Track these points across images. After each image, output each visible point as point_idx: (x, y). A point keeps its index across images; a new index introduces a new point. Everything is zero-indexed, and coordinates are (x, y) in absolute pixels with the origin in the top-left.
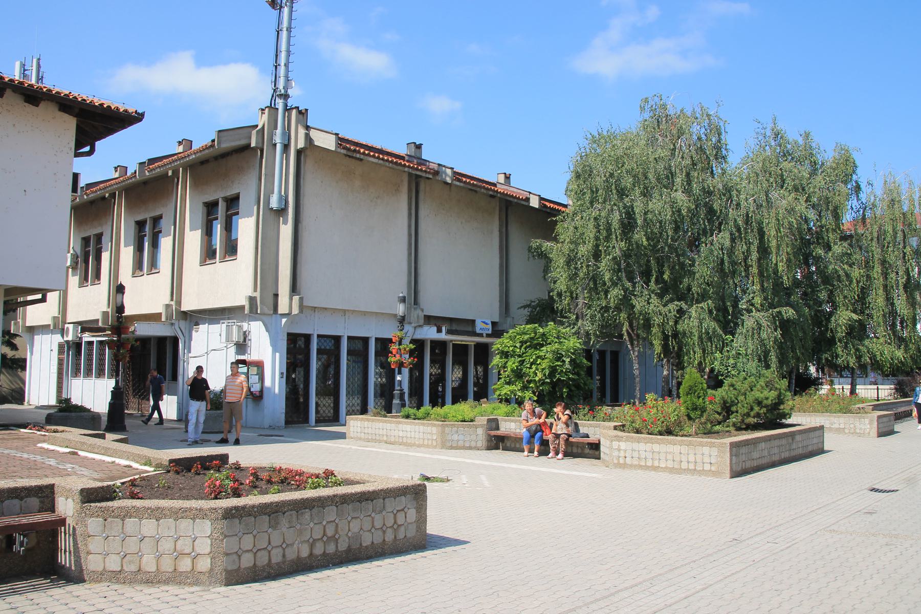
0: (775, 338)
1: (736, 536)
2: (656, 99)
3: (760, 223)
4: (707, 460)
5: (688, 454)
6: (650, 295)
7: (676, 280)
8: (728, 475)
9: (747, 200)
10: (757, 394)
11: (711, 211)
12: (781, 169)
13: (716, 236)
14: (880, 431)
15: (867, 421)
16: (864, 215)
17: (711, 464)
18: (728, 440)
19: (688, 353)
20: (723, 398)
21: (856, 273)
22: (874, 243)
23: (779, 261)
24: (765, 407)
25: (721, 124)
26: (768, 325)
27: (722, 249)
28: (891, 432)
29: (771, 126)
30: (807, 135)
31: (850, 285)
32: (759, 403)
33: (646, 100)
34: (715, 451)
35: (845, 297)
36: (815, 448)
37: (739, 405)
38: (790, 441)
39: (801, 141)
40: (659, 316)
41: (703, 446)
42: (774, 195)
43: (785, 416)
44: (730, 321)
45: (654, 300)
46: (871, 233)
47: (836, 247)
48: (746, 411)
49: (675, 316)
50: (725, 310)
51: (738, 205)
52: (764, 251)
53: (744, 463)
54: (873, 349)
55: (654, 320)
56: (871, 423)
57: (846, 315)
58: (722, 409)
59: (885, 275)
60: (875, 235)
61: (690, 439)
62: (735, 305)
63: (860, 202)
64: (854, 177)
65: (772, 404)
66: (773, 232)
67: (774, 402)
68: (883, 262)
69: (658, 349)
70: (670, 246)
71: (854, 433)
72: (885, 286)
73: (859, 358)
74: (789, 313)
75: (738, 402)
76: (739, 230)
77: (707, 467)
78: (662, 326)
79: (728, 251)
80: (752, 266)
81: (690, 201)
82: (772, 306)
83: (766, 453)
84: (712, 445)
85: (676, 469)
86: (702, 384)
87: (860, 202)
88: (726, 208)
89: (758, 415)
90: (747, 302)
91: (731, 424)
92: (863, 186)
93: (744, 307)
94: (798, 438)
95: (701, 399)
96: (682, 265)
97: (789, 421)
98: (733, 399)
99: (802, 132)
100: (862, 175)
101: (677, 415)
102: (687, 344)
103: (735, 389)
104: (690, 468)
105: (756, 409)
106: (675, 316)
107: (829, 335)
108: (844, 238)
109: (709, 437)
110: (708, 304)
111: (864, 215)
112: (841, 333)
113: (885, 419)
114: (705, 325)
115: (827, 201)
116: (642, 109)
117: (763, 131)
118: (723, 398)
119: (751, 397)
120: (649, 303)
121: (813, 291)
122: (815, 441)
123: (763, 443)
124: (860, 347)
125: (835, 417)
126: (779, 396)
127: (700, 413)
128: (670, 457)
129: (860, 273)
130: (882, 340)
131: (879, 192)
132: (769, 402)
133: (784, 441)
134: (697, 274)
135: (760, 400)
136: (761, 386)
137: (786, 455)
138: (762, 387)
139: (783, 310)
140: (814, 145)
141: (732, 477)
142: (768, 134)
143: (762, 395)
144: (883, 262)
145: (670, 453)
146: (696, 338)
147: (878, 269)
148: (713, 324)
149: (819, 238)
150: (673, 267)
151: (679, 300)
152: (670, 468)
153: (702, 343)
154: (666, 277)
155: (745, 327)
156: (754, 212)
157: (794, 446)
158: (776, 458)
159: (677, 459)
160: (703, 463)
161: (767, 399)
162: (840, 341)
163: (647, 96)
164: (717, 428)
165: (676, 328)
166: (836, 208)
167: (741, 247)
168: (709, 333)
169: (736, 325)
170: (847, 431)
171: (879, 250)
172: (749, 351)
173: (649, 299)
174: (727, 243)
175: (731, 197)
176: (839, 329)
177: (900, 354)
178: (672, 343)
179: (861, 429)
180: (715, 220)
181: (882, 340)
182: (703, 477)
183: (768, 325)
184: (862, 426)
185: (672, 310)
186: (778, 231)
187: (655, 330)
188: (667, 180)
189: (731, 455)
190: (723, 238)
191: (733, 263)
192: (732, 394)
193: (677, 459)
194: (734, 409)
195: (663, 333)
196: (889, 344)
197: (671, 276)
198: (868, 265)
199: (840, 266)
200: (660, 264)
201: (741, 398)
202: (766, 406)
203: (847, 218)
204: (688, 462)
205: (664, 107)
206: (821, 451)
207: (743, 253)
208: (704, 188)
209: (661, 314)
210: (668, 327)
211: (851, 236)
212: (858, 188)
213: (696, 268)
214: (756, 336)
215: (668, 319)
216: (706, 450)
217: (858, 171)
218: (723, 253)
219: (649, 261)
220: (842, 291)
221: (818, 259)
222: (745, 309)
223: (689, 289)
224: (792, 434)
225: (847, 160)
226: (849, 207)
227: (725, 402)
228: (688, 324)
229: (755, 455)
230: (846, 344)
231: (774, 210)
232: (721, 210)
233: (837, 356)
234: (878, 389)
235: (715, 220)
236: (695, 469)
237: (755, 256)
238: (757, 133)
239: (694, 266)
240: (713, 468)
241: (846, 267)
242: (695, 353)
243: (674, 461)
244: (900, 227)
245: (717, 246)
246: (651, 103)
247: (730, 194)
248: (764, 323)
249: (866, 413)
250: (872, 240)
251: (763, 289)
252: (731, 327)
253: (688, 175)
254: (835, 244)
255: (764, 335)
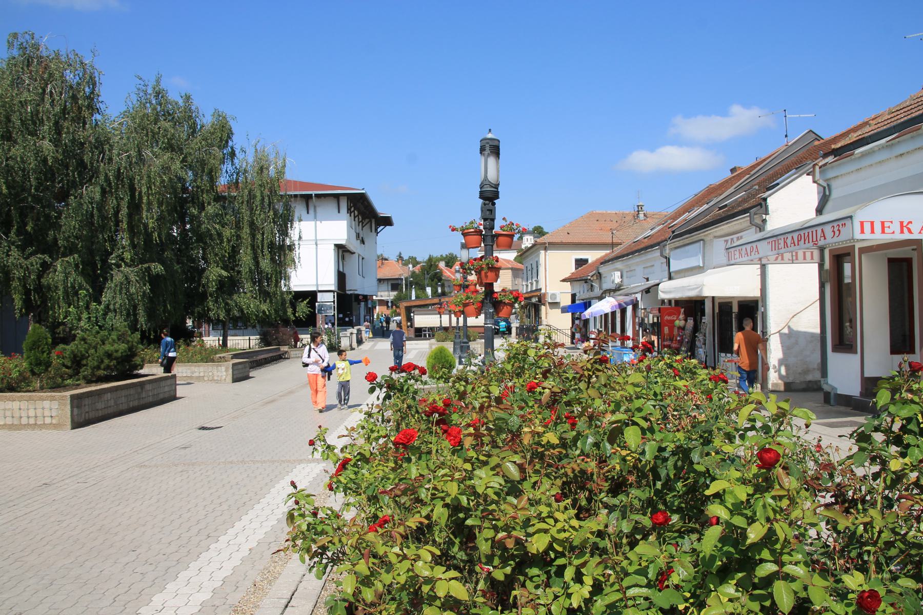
0: (144, 292)
1: (47, 481)
2: (27, 37)
3: (132, 180)
4: (47, 413)
5: (28, 409)
6: (9, 247)
7: (41, 231)
8: (69, 427)
9: (119, 155)
10: (108, 347)
11: (81, 164)
12: (159, 128)
13: (86, 189)
14: (235, 377)
15: (223, 369)
16: (237, 180)
17: (52, 417)
18: (68, 394)
19: (53, 308)
20: (73, 352)
21: (227, 232)
22: (244, 206)
23: (149, 218)
24: (115, 359)
25: (96, 74)
26: (136, 280)
27: (91, 203)
28: (247, 377)
29: (152, 83)
30: (188, 98)
31: (221, 243)
32: (109, 355)
33: (15, 36)
34: (55, 405)
35: (216, 255)
36: (166, 395)
37: (90, 358)
38: (139, 390)
39: (181, 102)
40: (20, 269)
41: (43, 400)
42: (147, 153)
43: (136, 367)
44: (99, 275)
45: (15, 252)
46: (242, 197)
47: (209, 207)
48: (96, 364)
49: (38, 269)
50: (94, 265)
51: (110, 159)
52: (135, 207)
53: (87, 415)
54: (240, 303)
55: (14, 274)
56: (226, 371)
57: (216, 271)
58: (73, 363)
59: (253, 236)
60: (246, 198)
61: (33, 394)
62: (104, 261)
63: (234, 167)
64: (230, 143)
65: (122, 356)
66: (144, 189)
67: (124, 354)
68: (252, 224)
69: (18, 302)
70: (33, 196)
71: (213, 380)
72: (253, 246)
73: (228, 311)
74: (157, 268)
75: (89, 356)
76: (110, 184)
77: (48, 420)
78: (23, 280)
79: (97, 205)
80: (122, 222)
81: (57, 151)
82: (142, 261)
83: (112, 403)
84: (52, 399)
85: (16, 425)
86: (46, 339)
87: (234, 167)
88: (98, 161)
89: (108, 367)
90: (117, 257)
91: (81, 377)
92: (237, 152)
93: (113, 262)
94: (148, 387)
95: (45, 354)
96: (48, 217)
97: (141, 372)
98: (84, 352)
99: (183, 94)
100: (237, 142)
101: (19, 371)
102: (52, 298)
103: (86, 343)
104: (31, 423)
105: (106, 361)
106: (38, 269)
107: (201, 289)
108: (219, 198)
109: (54, 392)
110: (74, 258)
111: (237, 180)
112: (212, 287)
113: (240, 366)
114: (71, 279)
115: (203, 163)
116: (10, 45)
117: (144, 88)
118: (73, 352)
119: (102, 350)
120: (8, 255)
121: (187, 248)
122: (167, 389)
123: (109, 394)
124: (229, 302)
125: (195, 366)
126: (130, 349)
127: (44, 368)
128: (8, 413)
129: (231, 233)
130: (249, 295)
131: (251, 159)
132: (119, 354)
133: (132, 391)
134: (63, 228)
135: (110, 352)
136: (112, 339)
137: (136, 403)
138: (114, 340)
139: (153, 265)
140: (193, 108)
141: (73, 428)
142: (150, 91)
143: (112, 348)
144: (252, 224)
145: (9, 409)
146: (60, 293)
147: (246, 230)
148: (80, 279)
149: (195, 200)
150: (38, 219)
151: (43, 253)
152: (9, 425)
153: (68, 297)
154: (29, 228)
155: (114, 281)
156: (125, 168)
157: (144, 395)
158: (124, 407)
159: (17, 415)
160: (44, 417)
161: (117, 351)
162: (211, 295)
163: (17, 32)
164: (69, 381)
165: (40, 282)
166: (211, 171)
167: (112, 202)
168: (75, 288)
169: (106, 280)
170: (206, 379)
171: (248, 213)
172: (117, 306)
173: (8, 251)
174: (98, 197)
175: (103, 152)
176: (210, 285)
177: (264, 307)
178: (34, 297)
179: (218, 376)
180: (86, 173)
181: (249, 295)
182: (44, 430)
183: (136, 280)
184: (219, 374)
185: (34, 263)
186: (149, 188)
187: (16, 284)
188: (32, 125)
189: (72, 407)
190: (92, 192)
191: (103, 217)
192: (82, 348)
193: (17, 415)
194: (84, 362)
195: (24, 286)
196: (255, 298)
197: (36, 228)
198: (238, 227)
199: (213, 226)
200: (23, 215)
201: (92, 351)
202: (116, 359)
203: (223, 181)
204: (28, 417)
205: (36, 47)
206: (174, 398)
207: (113, 208)
208: (74, 139)
209: (22, 267)
210: (29, 281)
211: (224, 198)
212: (233, 154)
213: (63, 221)
214: (124, 291)
215: (29, 273)
216: (47, 404)
217: (234, 138)
218: (93, 207)
219: (10, 210)
220: (213, 248)
221: (193, 218)
222: (114, 264)
223: (55, 240)
224: (142, 384)
225: (223, 127)
226: (224, 171)
227: (75, 356)
228: (53, 279)
229: (100, 405)
230: (217, 298)
231: (146, 168)
232: (93, 163)
233: (209, 310)
234: (249, 339)
235: (86, 173)
236: (36, 424)
237: (124, 211)
238: (139, 89)
239: (60, 218)
240: (54, 421)
241: (217, 226)
242: (59, 307)
243: (13, 417)
244: (267, 192)
245: (86, 199)
246: (21, 40)
247: (103, 148)
248: (133, 278)
249: (226, 361)
250: (242, 203)
251: (134, 246)
252: (100, 282)
253: (56, 123)
254: (209, 204)
255: (133, 290)
